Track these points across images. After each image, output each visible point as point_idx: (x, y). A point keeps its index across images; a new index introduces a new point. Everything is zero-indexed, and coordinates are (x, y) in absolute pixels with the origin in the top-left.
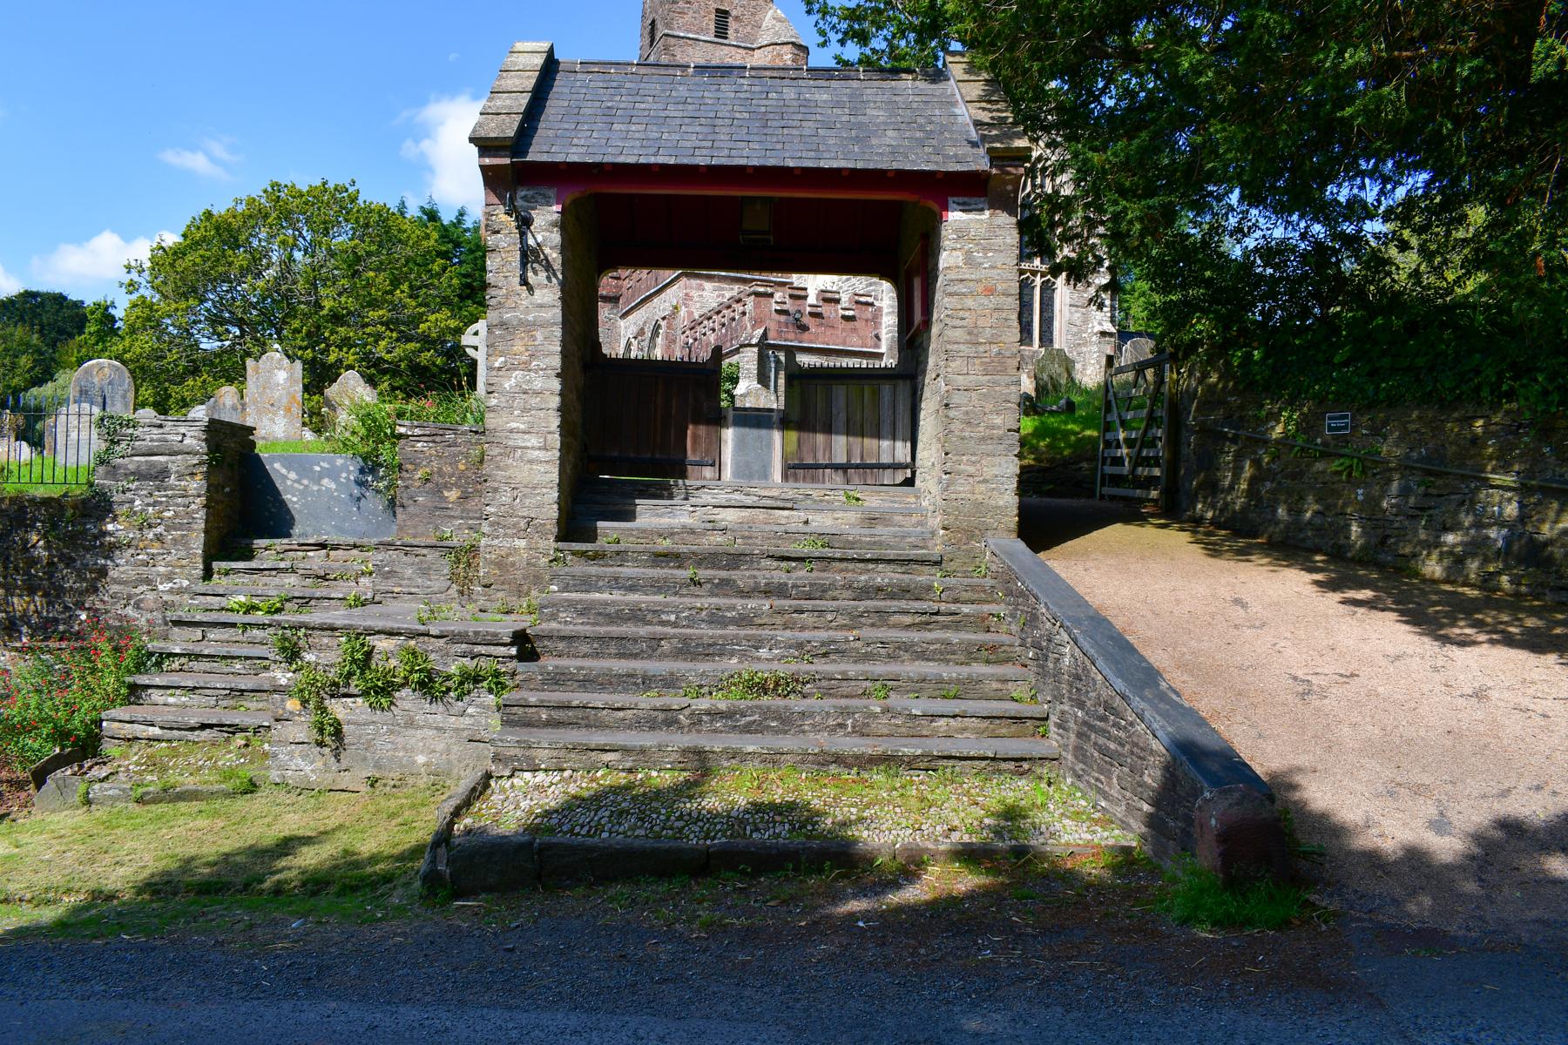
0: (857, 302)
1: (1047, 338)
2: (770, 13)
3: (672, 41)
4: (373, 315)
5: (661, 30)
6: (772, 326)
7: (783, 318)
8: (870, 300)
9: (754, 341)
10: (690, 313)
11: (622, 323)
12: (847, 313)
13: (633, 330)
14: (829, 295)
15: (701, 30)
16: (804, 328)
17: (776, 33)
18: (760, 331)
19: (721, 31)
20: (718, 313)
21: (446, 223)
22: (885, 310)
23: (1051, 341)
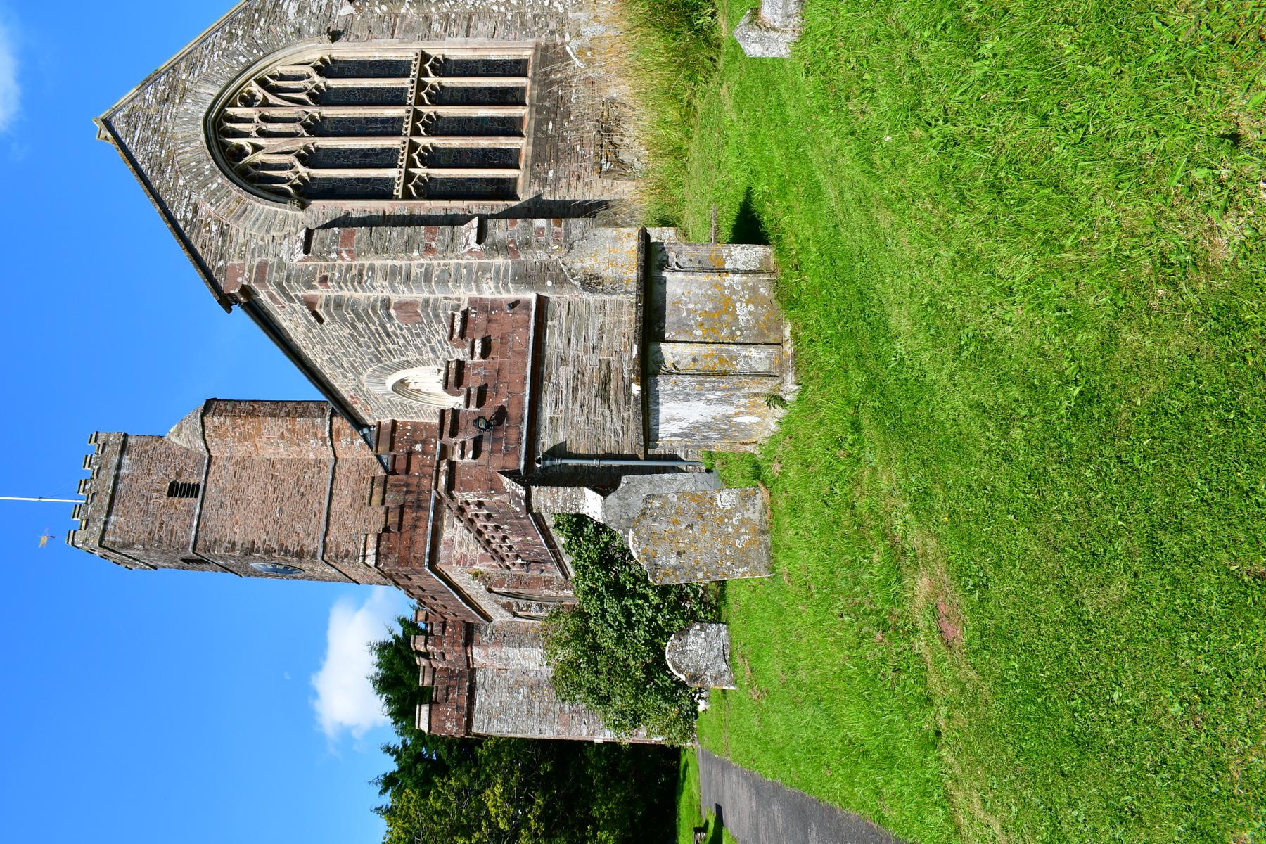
0: (463, 334)
1: (515, 68)
2: (173, 439)
3: (200, 543)
5: (189, 553)
6: (498, 463)
7: (486, 447)
9: (521, 491)
12: (478, 350)
14: (452, 376)
15: (190, 512)
16: (501, 414)
17: (193, 433)
18: (506, 482)
19: (191, 491)
21: (396, 768)
22: (474, 294)
23: (518, 63)
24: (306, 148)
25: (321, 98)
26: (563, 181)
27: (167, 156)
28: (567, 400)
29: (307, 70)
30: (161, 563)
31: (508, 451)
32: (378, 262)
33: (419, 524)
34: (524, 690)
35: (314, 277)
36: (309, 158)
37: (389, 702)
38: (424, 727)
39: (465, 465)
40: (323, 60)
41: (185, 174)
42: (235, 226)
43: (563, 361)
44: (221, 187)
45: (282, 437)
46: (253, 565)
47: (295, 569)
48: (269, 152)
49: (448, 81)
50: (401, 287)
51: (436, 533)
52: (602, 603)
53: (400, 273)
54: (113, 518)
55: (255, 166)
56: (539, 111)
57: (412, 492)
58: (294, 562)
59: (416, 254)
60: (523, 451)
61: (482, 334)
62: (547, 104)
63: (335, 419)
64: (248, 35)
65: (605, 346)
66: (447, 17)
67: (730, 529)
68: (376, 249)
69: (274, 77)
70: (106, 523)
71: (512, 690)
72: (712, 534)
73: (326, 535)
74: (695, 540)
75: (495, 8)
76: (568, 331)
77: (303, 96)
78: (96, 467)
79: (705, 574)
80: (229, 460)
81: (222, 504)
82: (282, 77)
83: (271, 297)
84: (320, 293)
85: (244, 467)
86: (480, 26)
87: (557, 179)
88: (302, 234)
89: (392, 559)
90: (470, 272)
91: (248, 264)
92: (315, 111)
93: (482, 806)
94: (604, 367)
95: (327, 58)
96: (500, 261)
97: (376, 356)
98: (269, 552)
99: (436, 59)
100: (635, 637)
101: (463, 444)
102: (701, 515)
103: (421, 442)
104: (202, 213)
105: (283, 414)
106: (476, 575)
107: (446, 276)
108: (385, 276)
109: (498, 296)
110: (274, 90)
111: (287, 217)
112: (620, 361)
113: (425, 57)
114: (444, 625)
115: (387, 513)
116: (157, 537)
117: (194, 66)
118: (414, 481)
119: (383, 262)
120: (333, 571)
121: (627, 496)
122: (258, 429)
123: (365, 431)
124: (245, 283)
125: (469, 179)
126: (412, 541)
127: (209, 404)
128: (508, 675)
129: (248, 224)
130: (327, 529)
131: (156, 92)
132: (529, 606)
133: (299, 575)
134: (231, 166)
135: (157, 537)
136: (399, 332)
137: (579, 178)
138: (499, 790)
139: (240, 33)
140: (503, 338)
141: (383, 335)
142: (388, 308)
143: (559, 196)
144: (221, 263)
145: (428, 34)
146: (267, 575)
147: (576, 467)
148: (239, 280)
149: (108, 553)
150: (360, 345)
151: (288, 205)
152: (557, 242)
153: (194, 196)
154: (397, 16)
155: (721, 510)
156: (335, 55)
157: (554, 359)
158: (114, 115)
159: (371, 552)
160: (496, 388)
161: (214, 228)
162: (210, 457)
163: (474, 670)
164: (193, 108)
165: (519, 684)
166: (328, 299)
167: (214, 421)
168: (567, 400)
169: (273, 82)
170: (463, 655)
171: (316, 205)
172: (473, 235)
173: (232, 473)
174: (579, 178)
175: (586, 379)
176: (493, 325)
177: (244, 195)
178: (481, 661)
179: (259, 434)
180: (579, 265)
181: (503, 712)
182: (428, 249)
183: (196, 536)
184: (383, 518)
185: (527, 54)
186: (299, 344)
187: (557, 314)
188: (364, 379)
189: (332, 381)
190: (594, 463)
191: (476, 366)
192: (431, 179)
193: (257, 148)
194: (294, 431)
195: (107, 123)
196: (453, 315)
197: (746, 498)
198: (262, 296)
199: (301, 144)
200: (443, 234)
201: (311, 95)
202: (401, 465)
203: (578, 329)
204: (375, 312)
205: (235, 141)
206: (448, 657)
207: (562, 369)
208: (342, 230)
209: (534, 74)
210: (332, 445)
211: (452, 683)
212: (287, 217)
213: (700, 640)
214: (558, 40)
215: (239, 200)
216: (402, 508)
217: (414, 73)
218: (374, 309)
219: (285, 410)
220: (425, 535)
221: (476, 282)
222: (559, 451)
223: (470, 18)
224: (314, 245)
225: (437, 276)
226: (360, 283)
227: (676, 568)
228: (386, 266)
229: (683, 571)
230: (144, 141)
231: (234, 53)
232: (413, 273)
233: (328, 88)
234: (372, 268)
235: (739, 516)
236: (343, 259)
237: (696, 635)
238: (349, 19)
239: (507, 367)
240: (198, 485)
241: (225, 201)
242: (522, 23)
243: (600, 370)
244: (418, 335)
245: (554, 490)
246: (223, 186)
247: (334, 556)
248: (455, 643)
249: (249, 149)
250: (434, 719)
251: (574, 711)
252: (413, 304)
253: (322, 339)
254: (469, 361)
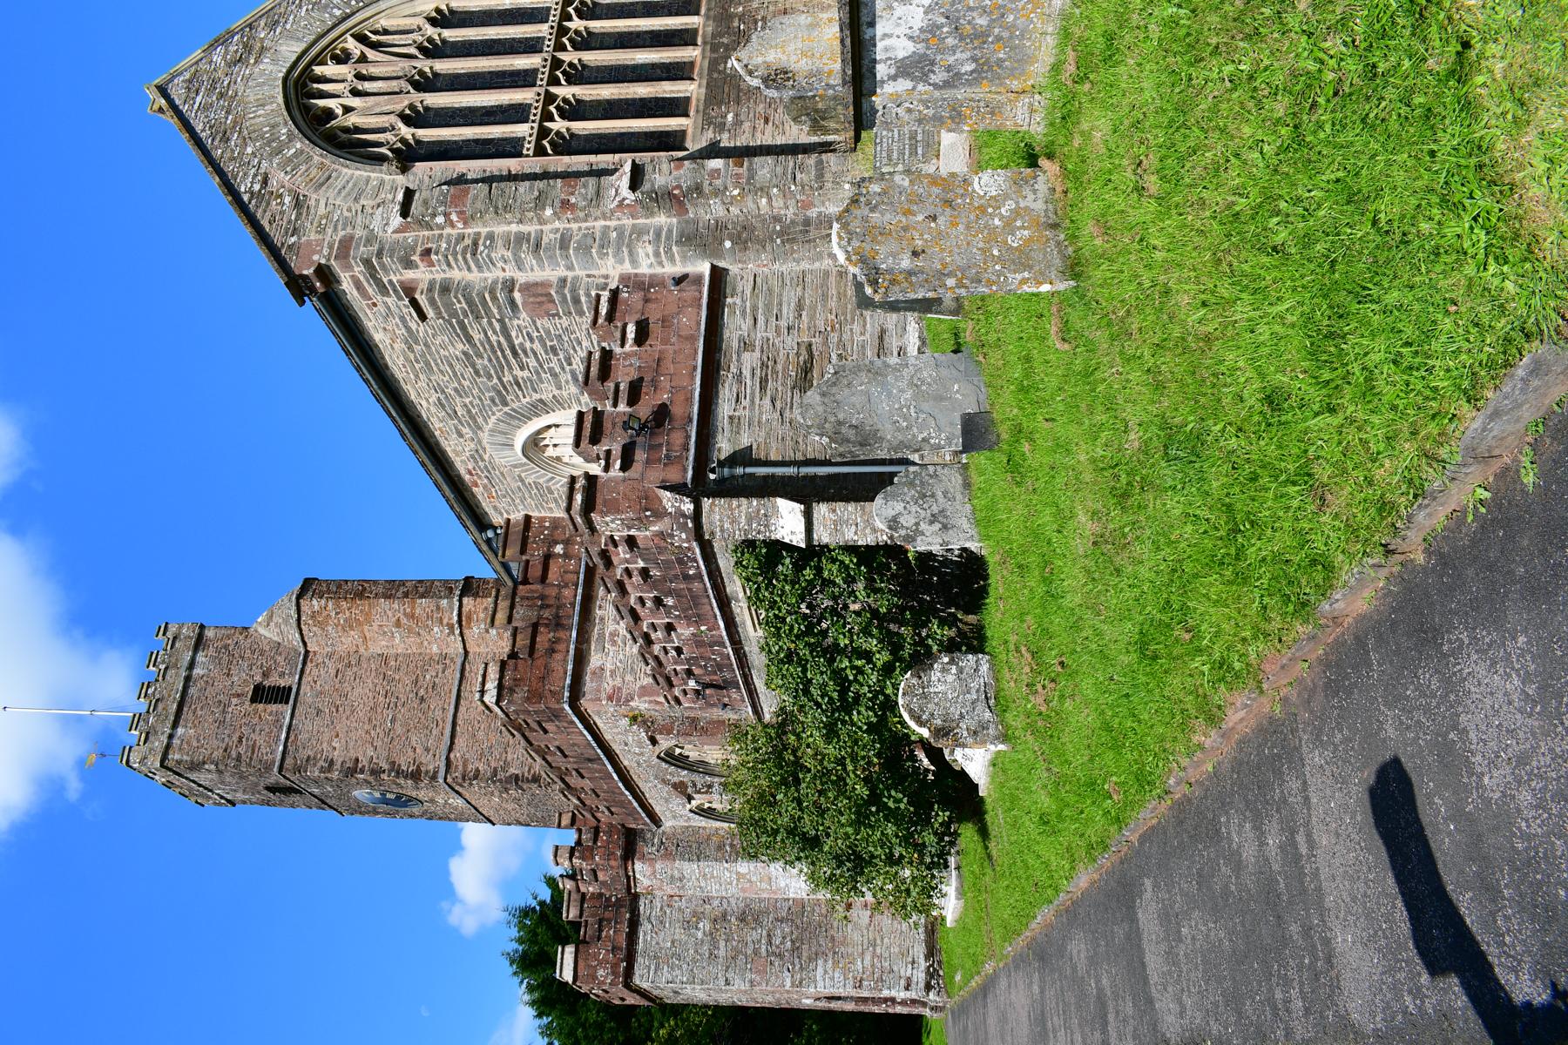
0: (610, 317)
2: (262, 631)
3: (289, 761)
5: (274, 777)
7: (640, 456)
8: (605, 295)
9: (688, 507)
10: (644, 691)
11: (668, 824)
13: (677, 802)
14: (594, 370)
15: (277, 722)
17: (286, 622)
19: (281, 695)
20: (648, 641)
22: (627, 268)
24: (412, 107)
25: (433, 50)
26: (746, 125)
27: (235, 122)
28: (753, 394)
29: (420, 21)
32: (500, 229)
33: (558, 647)
35: (414, 250)
36: (414, 118)
37: (530, 989)
38: (568, 976)
39: (610, 480)
40: (438, 10)
42: (314, 196)
43: (746, 345)
45: (398, 624)
46: (356, 793)
47: (411, 799)
48: (364, 115)
49: (597, 25)
50: (530, 260)
51: (581, 659)
52: (804, 671)
53: (528, 241)
54: (180, 731)
55: (346, 130)
56: (714, 48)
57: (548, 606)
58: (408, 787)
59: (549, 212)
60: (691, 458)
61: (637, 317)
62: (725, 40)
65: (804, 326)
67: (997, 222)
68: (496, 208)
69: (375, 32)
70: (171, 737)
71: (688, 925)
72: (968, 228)
73: (450, 749)
76: (755, 309)
77: (413, 51)
78: (162, 667)
81: (319, 712)
82: (386, 32)
83: (358, 285)
84: (421, 275)
85: (349, 665)
87: (738, 122)
88: (400, 197)
89: (520, 695)
90: (621, 236)
91: (328, 239)
92: (425, 65)
94: (804, 352)
95: (444, 7)
96: (662, 219)
97: (499, 393)
98: (377, 772)
101: (608, 453)
102: (948, 203)
103: (562, 542)
104: (274, 184)
105: (399, 594)
106: (634, 719)
107: (589, 241)
109: (658, 270)
110: (375, 46)
111: (382, 183)
112: (826, 342)
114: (596, 831)
115: (514, 635)
117: (277, 22)
118: (553, 592)
119: (506, 228)
120: (460, 802)
121: (834, 390)
123: (490, 534)
124: (323, 261)
125: (622, 135)
126: (548, 670)
127: (307, 587)
128: (683, 904)
129: (331, 193)
130: (452, 743)
131: (227, 52)
132: (710, 786)
133: (416, 810)
134: (314, 130)
136: (528, 345)
137: (767, 121)
140: (665, 321)
141: (508, 352)
142: (511, 291)
144: (293, 239)
146: (375, 812)
147: (766, 477)
148: (316, 257)
149: (172, 778)
150: (477, 372)
152: (737, 185)
153: (264, 164)
155: (981, 198)
157: (735, 344)
158: (171, 80)
159: (491, 686)
160: (655, 383)
161: (287, 200)
162: (307, 652)
163: (636, 897)
164: (271, 67)
166: (432, 284)
167: (312, 605)
168: (753, 394)
169: (374, 38)
170: (622, 872)
171: (420, 168)
173: (333, 672)
174: (767, 121)
175: (779, 367)
176: (650, 305)
177: (329, 160)
179: (369, 621)
180: (760, 60)
182: (565, 204)
184: (509, 643)
187: (739, 289)
188: (485, 437)
189: (444, 443)
191: (627, 355)
192: (572, 135)
193: (347, 110)
194: (412, 616)
195: (163, 91)
197: (1019, 183)
198: (346, 285)
199: (406, 103)
200: (585, 186)
202: (535, 572)
203: (768, 307)
204: (494, 298)
205: (321, 103)
206: (601, 876)
207: (746, 356)
209: (709, 10)
210: (461, 634)
211: (607, 914)
212: (382, 183)
213: (950, 678)
215: (322, 166)
216: (535, 626)
217: (554, 18)
218: (492, 292)
219: (402, 589)
220: (565, 661)
221: (628, 246)
222: (742, 457)
224: (416, 208)
225: (578, 242)
227: (910, 273)
228: (509, 233)
229: (922, 277)
230: (205, 108)
234: (491, 236)
236: (453, 225)
237: (944, 670)
239: (669, 356)
240: (290, 688)
241: (303, 168)
244: (554, 350)
245: (735, 502)
246: (302, 152)
247: (458, 778)
249: (339, 111)
250: (581, 964)
252: (545, 284)
253: (427, 364)
254: (617, 350)
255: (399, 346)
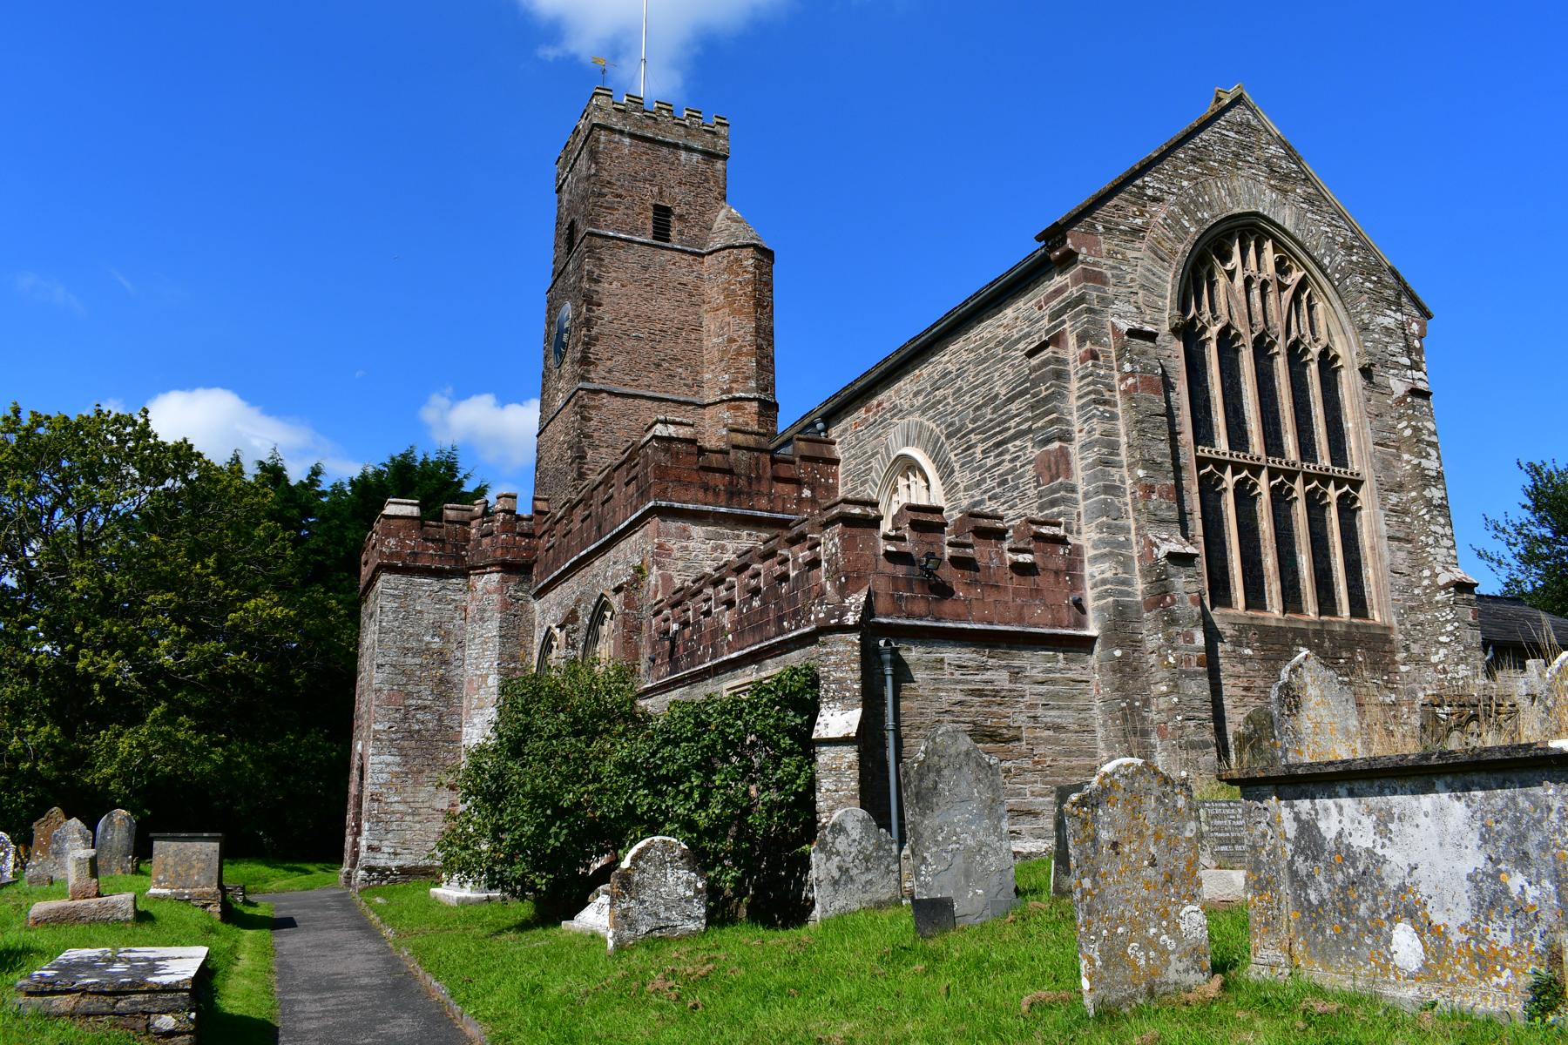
0: (1038, 537)
1: (1359, 605)
2: (722, 213)
3: (599, 241)
4: (154, 599)
5: (583, 228)
7: (901, 571)
8: (1061, 532)
9: (851, 619)
10: (667, 579)
11: (537, 606)
12: (1022, 558)
13: (557, 614)
14: (985, 523)
17: (732, 235)
21: (293, 482)
22: (1089, 553)
24: (1238, 336)
25: (1296, 355)
26: (1241, 669)
27: (1212, 169)
28: (967, 682)
29: (1324, 340)
30: (566, 197)
31: (896, 600)
32: (1121, 426)
33: (710, 494)
34: (437, 643)
36: (1227, 340)
37: (378, 474)
38: (390, 510)
39: (876, 541)
40: (1336, 357)
41: (1195, 187)
42: (1144, 246)
43: (1016, 675)
44: (1186, 231)
45: (731, 340)
47: (562, 356)
49: (1333, 514)
50: (1092, 456)
51: (698, 517)
52: (688, 740)
54: (627, 141)
55: (1211, 274)
56: (1317, 633)
57: (750, 484)
58: (574, 354)
59: (1141, 473)
61: (1040, 564)
62: (1327, 644)
63: (755, 404)
64: (1353, 269)
65: (1038, 733)
66: (1406, 512)
68: (1142, 422)
69: (1309, 298)
70: (621, 132)
71: (437, 628)
72: (1145, 900)
73: (610, 393)
74: (1135, 871)
75: (1427, 573)
76: (1053, 682)
77: (1294, 335)
79: (1089, 892)
80: (700, 277)
81: (645, 268)
82: (1311, 308)
85: (691, 295)
86: (1402, 555)
87: (1243, 660)
88: (1148, 328)
89: (662, 458)
91: (1103, 261)
92: (1281, 347)
93: (255, 592)
94: (1012, 733)
96: (1139, 586)
97: (959, 430)
98: (588, 323)
99: (1355, 499)
100: (635, 790)
101: (903, 539)
102: (1170, 879)
103: (813, 496)
105: (760, 341)
106: (639, 570)
107: (1114, 514)
108: (1105, 433)
109: (1088, 584)
111: (1161, 310)
112: (1022, 755)
113: (1357, 484)
115: (721, 452)
116: (605, 190)
117: (1313, 205)
118: (764, 488)
119: (1122, 431)
120: (560, 403)
122: (739, 312)
123: (820, 426)
124: (1080, 257)
126: (688, 485)
128: (458, 622)
129: (1148, 262)
130: (617, 395)
132: (573, 647)
133: (552, 361)
135: (605, 190)
136: (1008, 457)
138: (279, 612)
139: (1354, 258)
140: (1036, 592)
141: (1000, 438)
142: (1060, 439)
143: (1224, 663)
144: (1100, 228)
145: (1390, 486)
146: (550, 323)
148: (1084, 250)
150: (978, 408)
151: (1175, 312)
152: (1179, 660)
153: (1173, 198)
154: (1398, 448)
155: (1177, 913)
156: (1343, 372)
157: (1017, 663)
158: (1248, 107)
159: (672, 430)
160: (974, 583)
161: (1139, 221)
162: (703, 255)
163: (466, 575)
165: (445, 638)
166: (1064, 362)
168: (967, 682)
169: (1304, 297)
170: (489, 561)
171: (1178, 347)
172: (1175, 547)
173: (684, 280)
174: (1247, 689)
175: (995, 709)
176: (1052, 579)
178: (480, 585)
179: (733, 313)
181: (407, 613)
182: (1149, 489)
183: (607, 237)
185: (1376, 617)
186: (972, 334)
188: (915, 418)
190: (890, 723)
191: (1001, 555)
192: (1220, 494)
193: (1231, 275)
195: (1238, 101)
196: (1058, 525)
200: (1169, 508)
201: (1297, 342)
202: (784, 471)
203: (1055, 696)
204: (1052, 422)
205: (1236, 249)
207: (1005, 675)
208: (1158, 378)
210: (722, 401)
212: (1161, 310)
214: (1400, 656)
216: (729, 471)
217: (1337, 471)
220: (696, 502)
221: (1111, 553)
222: (903, 673)
223: (1410, 542)
224: (1138, 343)
225: (1112, 502)
226: (1095, 401)
227: (1095, 840)
228: (1118, 435)
229: (1090, 852)
230: (1224, 141)
231: (1332, 250)
232: (1113, 471)
233: (1306, 364)
234: (1114, 417)
235: (1171, 945)
236: (1122, 380)
237: (689, 883)
238: (1386, 391)
240: (668, 241)
241: (1171, 235)
242: (1412, 608)
243: (1009, 727)
245: (856, 666)
246: (1187, 233)
248: (506, 549)
249: (1229, 267)
250: (401, 523)
251: (407, 712)
252: (1068, 472)
253: (985, 360)
254: (1006, 545)
255: (1001, 333)
